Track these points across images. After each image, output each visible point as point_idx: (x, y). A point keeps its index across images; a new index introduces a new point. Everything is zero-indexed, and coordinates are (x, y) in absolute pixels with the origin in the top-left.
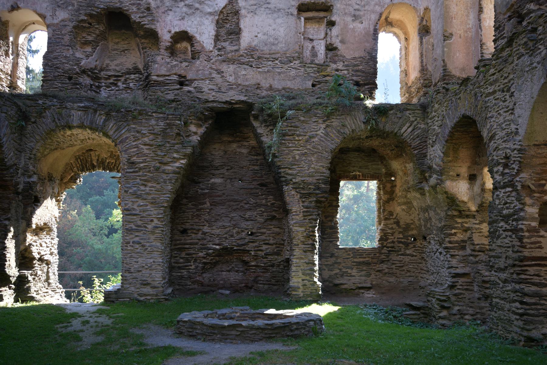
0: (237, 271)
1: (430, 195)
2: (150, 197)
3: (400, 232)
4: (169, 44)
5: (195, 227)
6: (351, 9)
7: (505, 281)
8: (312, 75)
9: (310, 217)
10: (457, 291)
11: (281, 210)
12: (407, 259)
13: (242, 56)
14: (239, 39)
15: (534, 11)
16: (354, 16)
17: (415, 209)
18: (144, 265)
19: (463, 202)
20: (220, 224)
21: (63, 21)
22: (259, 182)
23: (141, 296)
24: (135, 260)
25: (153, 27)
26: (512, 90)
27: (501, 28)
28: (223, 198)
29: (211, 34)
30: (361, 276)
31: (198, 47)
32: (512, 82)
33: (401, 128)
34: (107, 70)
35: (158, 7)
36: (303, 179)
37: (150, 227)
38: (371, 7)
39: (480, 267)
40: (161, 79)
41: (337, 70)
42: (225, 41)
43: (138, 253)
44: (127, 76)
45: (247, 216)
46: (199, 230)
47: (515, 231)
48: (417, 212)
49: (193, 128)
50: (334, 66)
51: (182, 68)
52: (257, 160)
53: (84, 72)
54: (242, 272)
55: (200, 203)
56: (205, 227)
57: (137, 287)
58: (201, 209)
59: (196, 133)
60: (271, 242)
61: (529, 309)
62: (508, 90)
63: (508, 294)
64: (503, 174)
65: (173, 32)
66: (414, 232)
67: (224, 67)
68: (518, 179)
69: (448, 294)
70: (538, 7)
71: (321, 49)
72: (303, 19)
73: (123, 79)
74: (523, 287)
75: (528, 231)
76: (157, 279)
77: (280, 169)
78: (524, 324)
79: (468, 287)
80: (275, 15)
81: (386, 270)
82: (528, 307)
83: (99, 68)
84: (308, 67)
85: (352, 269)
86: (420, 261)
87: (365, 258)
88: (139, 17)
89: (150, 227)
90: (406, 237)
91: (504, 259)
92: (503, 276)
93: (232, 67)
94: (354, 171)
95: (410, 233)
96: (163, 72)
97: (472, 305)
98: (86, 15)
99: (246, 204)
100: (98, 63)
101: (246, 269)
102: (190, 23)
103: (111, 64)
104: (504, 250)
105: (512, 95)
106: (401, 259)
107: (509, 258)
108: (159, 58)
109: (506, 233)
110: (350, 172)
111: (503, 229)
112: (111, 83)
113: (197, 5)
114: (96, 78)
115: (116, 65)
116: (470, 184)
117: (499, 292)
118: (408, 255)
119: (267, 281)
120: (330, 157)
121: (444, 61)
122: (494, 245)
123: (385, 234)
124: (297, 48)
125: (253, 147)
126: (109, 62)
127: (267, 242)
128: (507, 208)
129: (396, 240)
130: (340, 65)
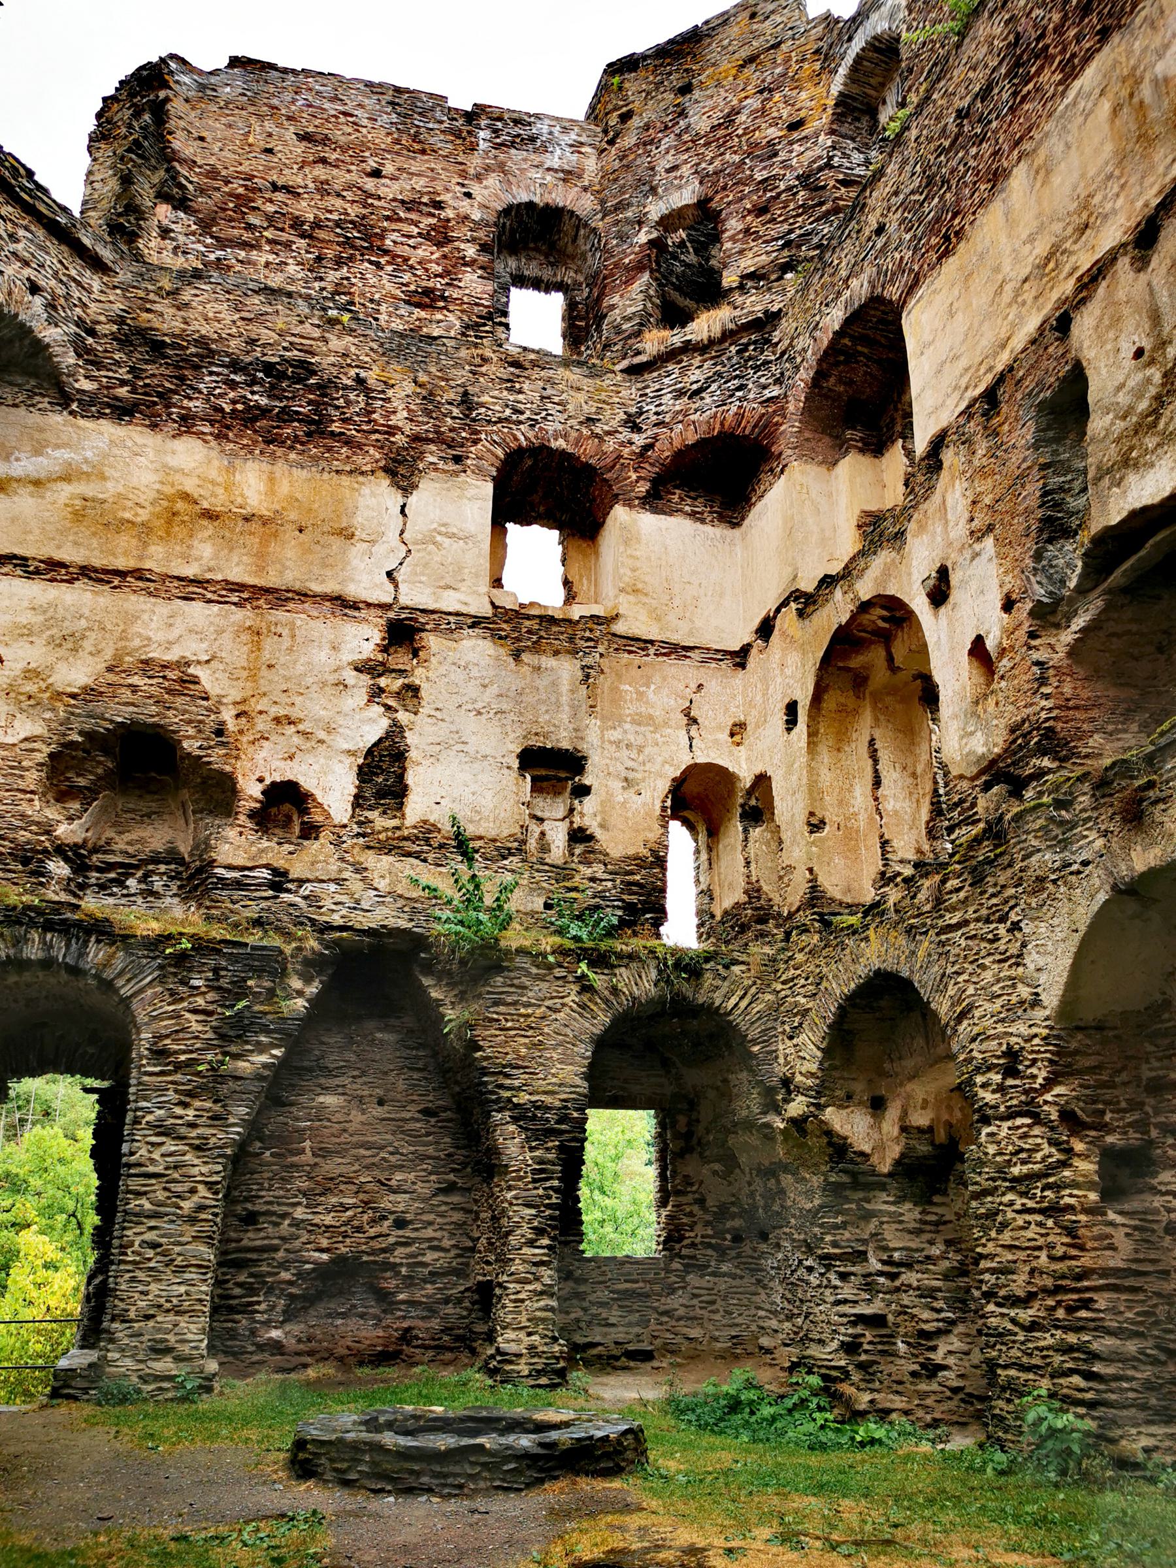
0: (362, 1316)
1: (785, 1140)
2: (194, 1133)
3: (707, 1224)
4: (258, 805)
5: (276, 1208)
6: (621, 768)
7: (1033, 1326)
8: (544, 885)
9: (548, 1184)
10: (863, 1357)
11: (469, 1170)
12: (723, 1284)
13: (405, 839)
14: (400, 806)
15: (1050, 771)
16: (626, 779)
17: (743, 1172)
18: (162, 1300)
19: (862, 1154)
20: (334, 1200)
21: (26, 739)
22: (422, 1106)
23: (146, 1382)
24: (141, 1288)
25: (228, 768)
26: (1013, 917)
27: (967, 804)
28: (342, 1139)
29: (346, 792)
30: (630, 1325)
31: (318, 818)
32: (1012, 903)
33: (727, 997)
34: (105, 852)
35: (241, 732)
36: (534, 1098)
37: (187, 1205)
38: (657, 767)
39: (906, 1299)
40: (236, 874)
41: (593, 879)
42: (371, 808)
43: (151, 1269)
44: (151, 867)
45: (393, 1183)
46: (284, 1216)
47: (1053, 1210)
48: (748, 1178)
49: (296, 983)
50: (588, 872)
51: (273, 851)
52: (417, 1057)
54: (375, 1317)
55: (290, 1151)
56: (300, 1209)
57: (140, 1357)
58: (293, 1165)
59: (300, 993)
60: (446, 1243)
61: (1106, 1392)
62: (1003, 919)
63: (1044, 1357)
64: (1001, 1089)
65: (268, 782)
66: (737, 1223)
67: (369, 859)
68: (1048, 1097)
69: (842, 1363)
70: (1054, 765)
71: (558, 836)
72: (529, 778)
73: (140, 874)
74: (1087, 1338)
75: (1087, 1211)
76: (190, 1336)
77: (485, 1075)
78: (1100, 1427)
79: (886, 1348)
80: (477, 766)
81: (681, 1312)
82: (1102, 1387)
83: (90, 845)
84: (538, 871)
85: (610, 1309)
86: (753, 1288)
87: (637, 1282)
88: (200, 748)
89: (187, 1205)
91: (1025, 1277)
92: (1025, 1315)
93: (387, 860)
94: (613, 1087)
95: (729, 1224)
96: (240, 862)
97: (900, 1388)
98: (81, 733)
99: (392, 1153)
100: (89, 834)
101: (384, 1311)
102: (304, 767)
103: (117, 839)
104: (1022, 1255)
105: (1016, 927)
106: (710, 1285)
107: (1042, 1273)
108: (231, 833)
109: (1028, 1217)
110: (605, 1090)
111: (1018, 1207)
112: (112, 880)
113: (322, 735)
115: (128, 843)
116: (873, 1116)
117: (1015, 1353)
118: (724, 1275)
119: (433, 1339)
120: (589, 1054)
121: (811, 870)
122: (990, 1244)
123: (677, 1226)
124: (517, 830)
125: (411, 1031)
126: (113, 835)
127: (436, 1243)
128: (1024, 1162)
129: (699, 1240)
130: (598, 870)
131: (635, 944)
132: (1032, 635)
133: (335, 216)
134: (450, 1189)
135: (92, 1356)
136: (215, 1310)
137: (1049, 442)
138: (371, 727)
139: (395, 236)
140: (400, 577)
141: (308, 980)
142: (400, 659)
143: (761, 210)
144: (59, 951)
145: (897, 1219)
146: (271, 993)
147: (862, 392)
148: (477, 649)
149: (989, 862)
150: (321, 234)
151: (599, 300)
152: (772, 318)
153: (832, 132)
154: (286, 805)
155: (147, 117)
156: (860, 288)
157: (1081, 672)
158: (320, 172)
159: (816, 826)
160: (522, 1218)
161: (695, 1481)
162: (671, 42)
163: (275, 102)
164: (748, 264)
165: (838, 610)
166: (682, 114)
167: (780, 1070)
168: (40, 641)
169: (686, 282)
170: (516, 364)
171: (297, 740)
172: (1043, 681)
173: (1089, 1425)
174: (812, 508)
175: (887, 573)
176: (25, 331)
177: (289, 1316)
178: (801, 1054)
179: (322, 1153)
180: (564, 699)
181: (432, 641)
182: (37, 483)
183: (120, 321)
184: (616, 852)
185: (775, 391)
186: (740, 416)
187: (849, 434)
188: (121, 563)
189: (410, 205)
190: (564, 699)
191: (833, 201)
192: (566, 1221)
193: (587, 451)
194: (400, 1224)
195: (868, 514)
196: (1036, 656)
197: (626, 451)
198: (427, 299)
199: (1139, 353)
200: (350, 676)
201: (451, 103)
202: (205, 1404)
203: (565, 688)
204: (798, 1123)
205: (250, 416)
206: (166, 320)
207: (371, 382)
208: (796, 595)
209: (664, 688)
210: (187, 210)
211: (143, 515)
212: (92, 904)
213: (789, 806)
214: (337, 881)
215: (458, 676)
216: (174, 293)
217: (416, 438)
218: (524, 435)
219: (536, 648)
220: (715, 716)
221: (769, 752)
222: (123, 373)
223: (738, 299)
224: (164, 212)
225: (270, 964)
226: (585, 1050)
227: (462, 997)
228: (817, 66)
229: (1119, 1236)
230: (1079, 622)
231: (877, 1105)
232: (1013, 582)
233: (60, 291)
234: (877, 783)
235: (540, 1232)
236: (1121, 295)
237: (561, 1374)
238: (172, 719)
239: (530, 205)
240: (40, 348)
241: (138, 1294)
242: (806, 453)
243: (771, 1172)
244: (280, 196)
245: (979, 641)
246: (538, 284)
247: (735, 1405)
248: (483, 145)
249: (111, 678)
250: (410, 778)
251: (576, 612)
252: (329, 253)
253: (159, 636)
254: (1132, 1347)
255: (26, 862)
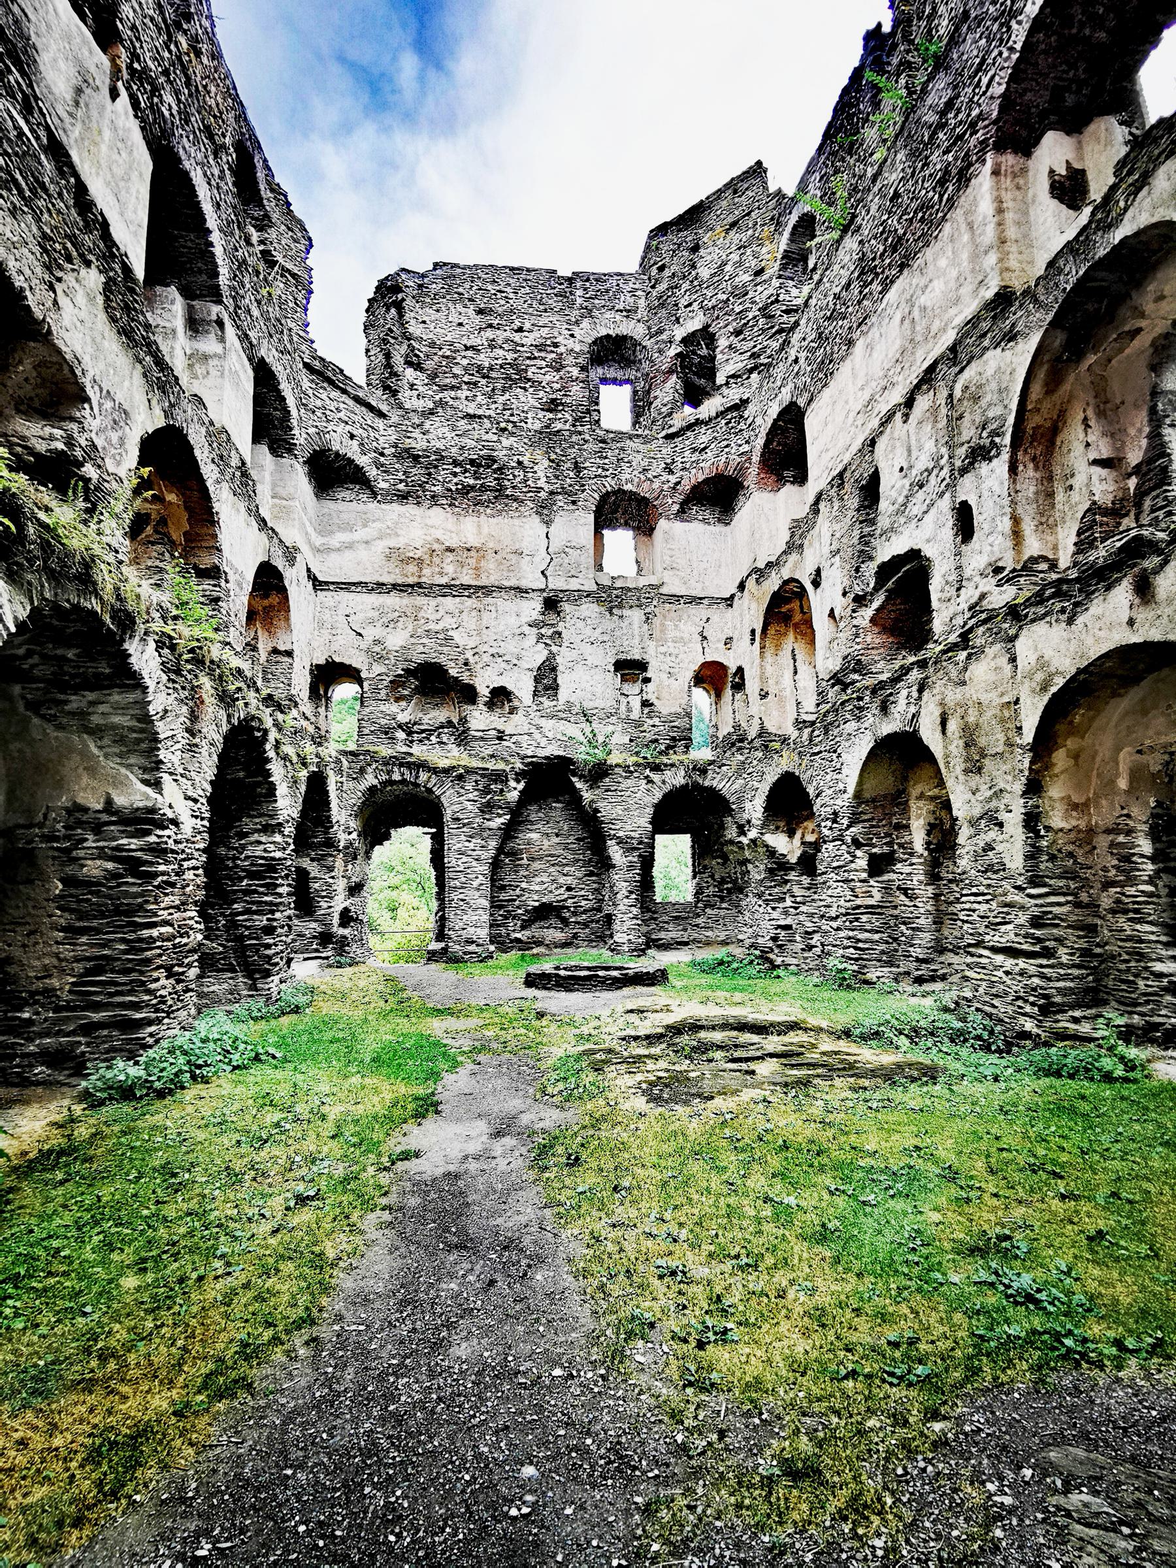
7: (838, 929)
12: (722, 913)
39: (801, 918)
49: (512, 784)
50: (651, 722)
53: (400, 726)
67: (543, 722)
71: (636, 703)
90: (721, 891)
92: (835, 924)
105: (839, 756)
108: (476, 714)
114: (410, 733)
130: (656, 721)
131: (674, 758)
132: (854, 611)
133: (500, 362)
134: (591, 874)
135: (443, 945)
136: (491, 926)
137: (865, 507)
138: (539, 656)
139: (533, 369)
140: (548, 573)
141: (518, 782)
142: (552, 618)
143: (737, 333)
144: (407, 777)
145: (799, 883)
146: (502, 790)
147: (786, 455)
148: (590, 609)
149: (831, 724)
150: (493, 374)
151: (648, 392)
152: (745, 402)
153: (780, 277)
154: (500, 696)
155: (393, 311)
156: (785, 396)
157: (876, 630)
158: (489, 334)
159: (764, 696)
160: (622, 887)
161: (685, 988)
162: (686, 212)
163: (461, 290)
164: (730, 368)
165: (773, 583)
166: (694, 267)
167: (746, 816)
168: (379, 624)
169: (697, 373)
170: (603, 441)
171: (504, 665)
172: (857, 635)
173: (856, 968)
174: (767, 512)
175: (795, 566)
176: (351, 461)
177: (523, 928)
178: (755, 809)
179: (532, 859)
180: (636, 632)
181: (566, 607)
182: (367, 542)
183: (396, 446)
184: (665, 712)
185: (746, 448)
186: (727, 463)
187: (785, 473)
188: (411, 581)
189: (541, 347)
190: (636, 632)
191: (779, 321)
192: (646, 884)
193: (645, 491)
194: (569, 889)
195: (794, 521)
196: (855, 622)
197: (665, 487)
198: (553, 406)
199: (902, 469)
200: (527, 629)
201: (560, 273)
202: (490, 963)
203: (636, 626)
204: (754, 841)
205: (466, 490)
206: (418, 443)
207: (526, 463)
208: (756, 570)
209: (688, 622)
210: (422, 370)
211: (418, 554)
212: (417, 750)
213: (752, 685)
214: (530, 734)
215: (581, 624)
216: (421, 425)
217: (552, 493)
218: (610, 484)
219: (620, 606)
220: (716, 635)
221: (741, 656)
222: (401, 476)
223: (725, 390)
224: (410, 373)
225: (499, 777)
226: (650, 811)
227: (591, 787)
228: (772, 228)
229: (875, 892)
230: (876, 604)
231: (791, 834)
232: (847, 582)
233: (365, 435)
234: (796, 673)
235: (631, 892)
236: (896, 435)
237: (643, 951)
238: (442, 660)
239: (608, 336)
240: (359, 469)
241: (456, 921)
242: (761, 485)
243: (745, 862)
244: (469, 353)
245: (832, 610)
246: (615, 381)
247: (721, 963)
248: (579, 301)
249: (413, 640)
250: (559, 681)
251: (642, 582)
252: (499, 386)
253: (433, 617)
254: (876, 937)
255: (386, 733)
